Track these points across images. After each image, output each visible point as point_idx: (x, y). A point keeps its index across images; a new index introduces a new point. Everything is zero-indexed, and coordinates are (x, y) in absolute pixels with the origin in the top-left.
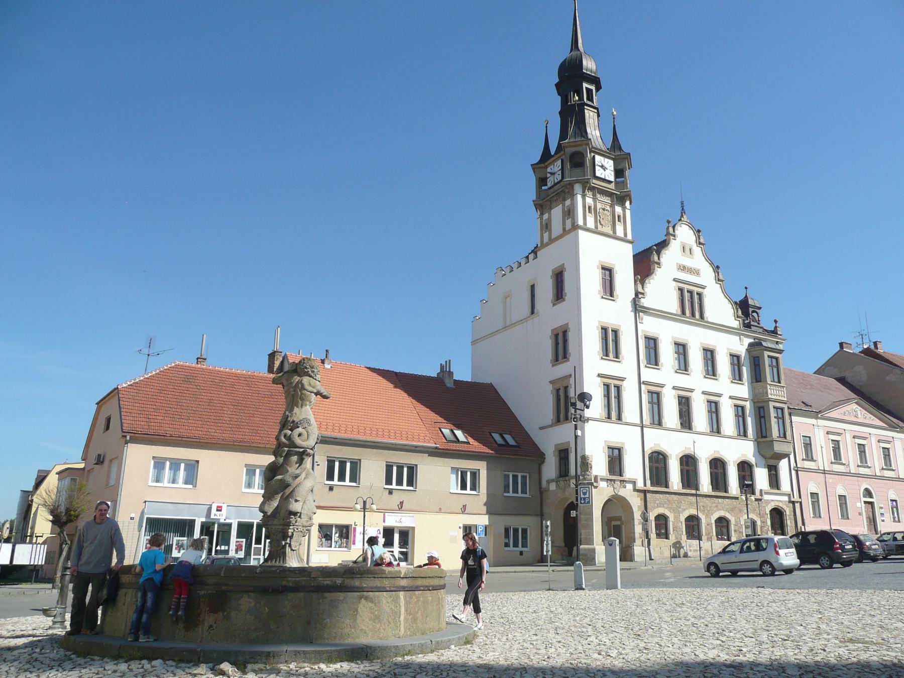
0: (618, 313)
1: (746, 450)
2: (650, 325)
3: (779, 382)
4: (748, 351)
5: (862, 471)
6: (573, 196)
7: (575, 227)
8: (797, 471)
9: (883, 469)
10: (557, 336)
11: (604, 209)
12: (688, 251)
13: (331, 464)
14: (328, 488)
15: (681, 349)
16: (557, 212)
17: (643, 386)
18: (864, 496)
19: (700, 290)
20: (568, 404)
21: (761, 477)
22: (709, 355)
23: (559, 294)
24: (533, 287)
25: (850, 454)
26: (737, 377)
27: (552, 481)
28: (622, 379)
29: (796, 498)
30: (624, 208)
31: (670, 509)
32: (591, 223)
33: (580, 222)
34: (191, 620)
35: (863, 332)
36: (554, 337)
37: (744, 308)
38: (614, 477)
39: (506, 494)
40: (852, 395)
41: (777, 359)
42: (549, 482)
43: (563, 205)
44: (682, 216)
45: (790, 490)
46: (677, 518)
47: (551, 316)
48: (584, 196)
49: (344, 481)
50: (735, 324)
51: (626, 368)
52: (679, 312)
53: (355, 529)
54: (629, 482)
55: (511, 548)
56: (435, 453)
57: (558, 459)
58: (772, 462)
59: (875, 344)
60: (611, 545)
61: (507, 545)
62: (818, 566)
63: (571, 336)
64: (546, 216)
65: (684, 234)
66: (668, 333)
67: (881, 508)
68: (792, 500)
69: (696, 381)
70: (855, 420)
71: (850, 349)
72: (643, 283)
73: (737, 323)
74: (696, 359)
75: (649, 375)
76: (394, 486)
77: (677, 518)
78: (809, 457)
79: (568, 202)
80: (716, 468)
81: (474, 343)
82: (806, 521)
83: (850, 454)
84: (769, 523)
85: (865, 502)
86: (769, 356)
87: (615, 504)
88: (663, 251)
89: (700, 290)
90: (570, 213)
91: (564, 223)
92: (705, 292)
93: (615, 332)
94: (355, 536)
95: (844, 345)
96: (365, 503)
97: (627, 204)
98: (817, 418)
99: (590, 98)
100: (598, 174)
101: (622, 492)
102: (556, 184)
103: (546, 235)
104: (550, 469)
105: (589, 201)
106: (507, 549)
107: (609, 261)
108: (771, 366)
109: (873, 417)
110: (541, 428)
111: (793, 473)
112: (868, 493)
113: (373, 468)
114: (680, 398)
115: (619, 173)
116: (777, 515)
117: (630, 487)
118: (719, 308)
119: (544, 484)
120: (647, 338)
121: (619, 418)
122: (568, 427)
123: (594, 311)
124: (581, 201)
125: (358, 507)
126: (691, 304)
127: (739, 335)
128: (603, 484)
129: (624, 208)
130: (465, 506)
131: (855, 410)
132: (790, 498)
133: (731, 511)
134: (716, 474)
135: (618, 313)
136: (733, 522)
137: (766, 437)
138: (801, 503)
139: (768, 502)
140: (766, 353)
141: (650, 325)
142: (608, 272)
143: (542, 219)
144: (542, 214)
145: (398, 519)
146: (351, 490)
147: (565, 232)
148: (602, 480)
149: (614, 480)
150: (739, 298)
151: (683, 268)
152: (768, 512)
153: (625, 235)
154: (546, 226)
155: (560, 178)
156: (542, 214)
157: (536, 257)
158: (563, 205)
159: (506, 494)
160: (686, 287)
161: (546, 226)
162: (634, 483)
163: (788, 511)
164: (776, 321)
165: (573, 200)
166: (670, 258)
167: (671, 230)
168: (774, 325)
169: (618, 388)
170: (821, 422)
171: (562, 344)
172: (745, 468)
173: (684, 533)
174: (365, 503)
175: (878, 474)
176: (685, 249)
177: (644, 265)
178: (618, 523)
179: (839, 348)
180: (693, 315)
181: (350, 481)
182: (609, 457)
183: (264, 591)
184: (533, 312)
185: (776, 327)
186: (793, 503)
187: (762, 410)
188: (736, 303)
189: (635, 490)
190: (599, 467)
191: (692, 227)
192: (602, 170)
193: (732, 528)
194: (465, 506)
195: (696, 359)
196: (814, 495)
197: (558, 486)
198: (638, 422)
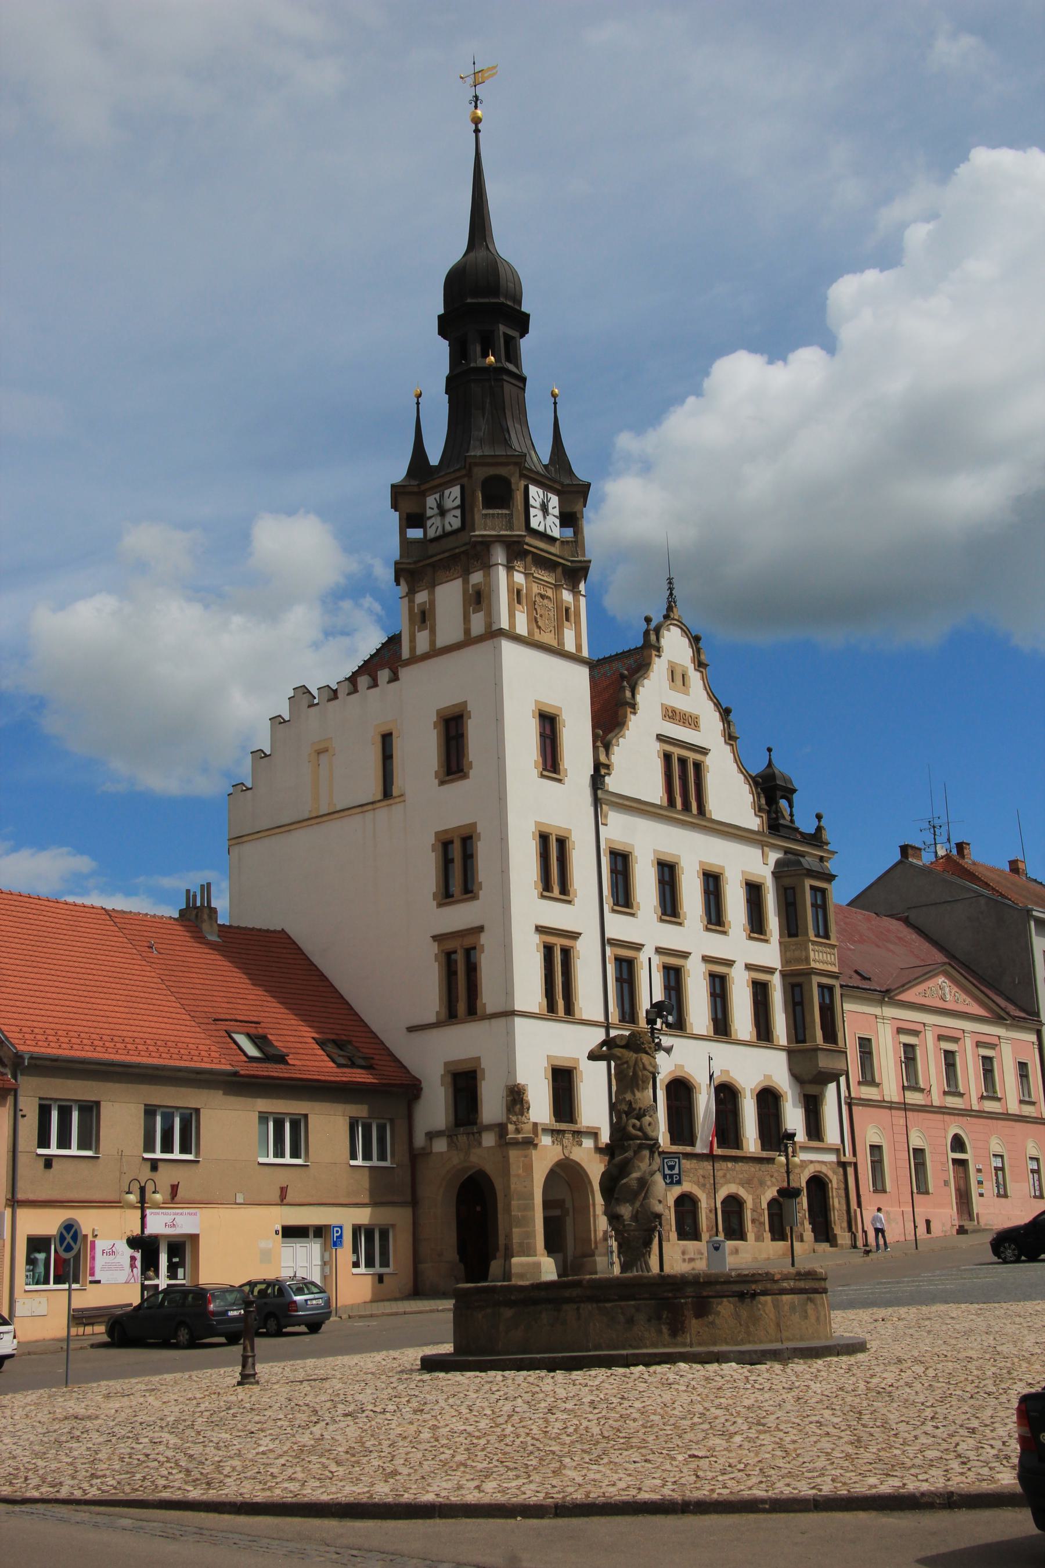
0: (566, 806)
2: (620, 829)
3: (827, 936)
4: (776, 875)
5: (952, 1102)
6: (487, 567)
8: (850, 1105)
9: (982, 1097)
11: (543, 597)
13: (44, 1112)
14: (148, 1164)
15: (668, 874)
16: (449, 596)
17: (608, 949)
18: (953, 1150)
19: (698, 757)
20: (463, 981)
21: (794, 1118)
22: (713, 883)
23: (454, 762)
24: (387, 739)
25: (931, 1069)
26: (757, 926)
27: (439, 1134)
28: (575, 936)
29: (848, 1157)
34: (677, 1329)
35: (937, 822)
37: (770, 789)
38: (563, 1126)
39: (262, 1160)
40: (940, 957)
41: (823, 891)
42: (431, 1136)
43: (466, 582)
45: (838, 1141)
46: (757, 1200)
47: (432, 805)
48: (510, 569)
49: (283, 1156)
50: (753, 822)
51: (580, 913)
52: (665, 803)
53: (93, 1244)
55: (362, 1269)
56: (238, 1084)
57: (450, 1090)
58: (812, 1090)
59: (960, 847)
60: (717, 1249)
61: (356, 1265)
63: (483, 851)
64: (421, 597)
66: (647, 841)
67: (979, 1171)
68: (843, 1159)
69: (691, 936)
70: (940, 1004)
72: (607, 747)
73: (758, 820)
75: (619, 927)
76: (53, 1150)
77: (757, 1200)
78: (869, 1079)
79: (476, 578)
83: (931, 1069)
85: (955, 1161)
86: (812, 887)
87: (566, 1174)
89: (698, 757)
90: (479, 599)
91: (466, 619)
92: (709, 761)
93: (562, 842)
94: (93, 1258)
95: (910, 851)
96: (142, 1190)
97: (582, 587)
98: (881, 1003)
100: (534, 524)
102: (446, 535)
104: (435, 1109)
105: (519, 578)
106: (356, 1271)
107: (552, 701)
108: (814, 905)
109: (968, 1000)
110: (411, 1029)
111: (844, 1108)
112: (958, 1144)
113: (122, 1117)
114: (667, 969)
115: (569, 519)
117: (588, 1143)
118: (730, 796)
119: (420, 1140)
121: (569, 1010)
123: (533, 804)
124: (504, 580)
125: (133, 1198)
126: (684, 786)
127: (762, 845)
128: (546, 1140)
129: (576, 592)
130: (283, 1191)
131: (942, 988)
132: (838, 1156)
133: (747, 1183)
135: (566, 806)
136: (749, 1204)
137: (804, 1041)
138: (855, 1164)
139: (804, 1164)
140: (809, 882)
141: (620, 829)
142: (549, 724)
143: (411, 601)
144: (411, 593)
145: (168, 1219)
146: (83, 1165)
147: (469, 641)
148: (545, 1130)
149: (563, 1132)
150: (758, 767)
151: (672, 715)
153: (579, 647)
155: (456, 523)
156: (411, 593)
158: (466, 582)
159: (353, 1163)
160: (677, 751)
161: (424, 617)
162: (595, 1135)
164: (819, 817)
165: (487, 575)
166: (653, 692)
167: (653, 637)
168: (816, 823)
169: (566, 952)
170: (890, 1012)
171: (459, 863)
173: (674, 1228)
174: (142, 1190)
175: (975, 1107)
176: (677, 678)
179: (898, 857)
180: (687, 807)
181: (80, 1148)
183: (741, 1296)
184: (387, 793)
185: (819, 829)
186: (843, 1165)
187: (797, 989)
188: (753, 779)
189: (598, 1150)
190: (540, 1107)
191: (686, 631)
193: (748, 1215)
194: (283, 1191)
196: (876, 1149)
197: (452, 1144)
198: (602, 1019)
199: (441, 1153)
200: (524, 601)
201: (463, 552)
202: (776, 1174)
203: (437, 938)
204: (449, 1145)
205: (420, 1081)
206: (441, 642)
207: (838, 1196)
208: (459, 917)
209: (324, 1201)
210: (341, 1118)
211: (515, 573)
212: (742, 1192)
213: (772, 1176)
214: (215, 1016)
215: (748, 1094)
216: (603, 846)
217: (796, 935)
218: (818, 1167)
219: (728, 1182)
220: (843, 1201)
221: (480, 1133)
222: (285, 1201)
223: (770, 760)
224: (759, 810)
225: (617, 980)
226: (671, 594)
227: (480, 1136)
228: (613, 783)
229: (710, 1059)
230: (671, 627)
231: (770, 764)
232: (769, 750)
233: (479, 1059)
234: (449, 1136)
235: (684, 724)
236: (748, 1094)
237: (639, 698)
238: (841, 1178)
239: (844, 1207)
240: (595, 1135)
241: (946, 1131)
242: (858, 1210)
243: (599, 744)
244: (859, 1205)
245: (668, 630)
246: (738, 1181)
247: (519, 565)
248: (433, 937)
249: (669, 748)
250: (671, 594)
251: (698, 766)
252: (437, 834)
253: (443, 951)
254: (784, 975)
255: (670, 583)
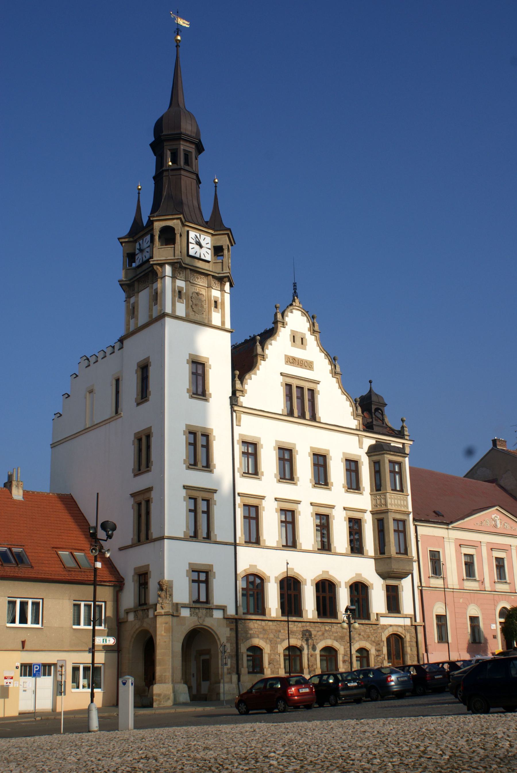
1: (365, 568)
2: (250, 427)
7: (163, 315)
10: (140, 440)
12: (298, 341)
15: (286, 456)
16: (143, 297)
17: (238, 499)
22: (320, 462)
23: (144, 394)
24: (117, 381)
26: (353, 484)
27: (184, 606)
30: (222, 290)
31: (265, 639)
32: (181, 309)
33: (168, 309)
36: (136, 442)
42: (127, 612)
44: (294, 300)
50: (354, 423)
54: (219, 608)
57: (137, 585)
62: (369, 699)
64: (132, 300)
65: (296, 321)
68: (414, 623)
69: (304, 492)
71: (505, 446)
72: (242, 378)
74: (304, 467)
77: (274, 648)
80: (324, 591)
81: (53, 446)
82: (429, 648)
84: (385, 650)
88: (268, 341)
90: (156, 298)
95: (498, 443)
99: (187, 162)
101: (208, 622)
103: (132, 322)
108: (393, 472)
111: (452, 590)
116: (396, 641)
118: (335, 404)
120: (245, 443)
122: (146, 549)
126: (301, 403)
129: (222, 290)
130: (23, 643)
134: (324, 598)
139: (385, 627)
149: (199, 608)
151: (292, 361)
152: (384, 639)
153: (223, 323)
154: (132, 312)
156: (129, 297)
157: (121, 348)
159: (75, 627)
161: (132, 312)
163: (408, 638)
164: (403, 421)
166: (277, 349)
168: (401, 424)
171: (145, 450)
172: (359, 590)
176: (298, 340)
177: (245, 359)
178: (207, 657)
181: (20, 622)
182: (147, 588)
184: (117, 412)
185: (403, 427)
192: (197, 247)
193: (340, 658)
194: (23, 643)
195: (304, 467)
197: (136, 616)
198: (233, 541)
199: (132, 621)
200: (183, 297)
201: (150, 271)
202: (362, 633)
203: (133, 495)
204: (135, 617)
205: (123, 579)
206: (141, 323)
207: (411, 646)
208: (143, 482)
209: (34, 649)
210: (67, 601)
211: (213, 290)
212: (336, 645)
213: (360, 634)
214: (52, 546)
215: (343, 585)
216: (236, 438)
217: (380, 490)
218: (395, 629)
219: (361, 639)
220: (415, 649)
221: (148, 609)
222: (24, 649)
223: (371, 387)
224: (355, 415)
225: (245, 517)
226: (295, 292)
227: (148, 611)
228: (243, 400)
229: (288, 564)
230: (294, 311)
231: (371, 391)
232: (370, 382)
233: (148, 565)
234: (135, 611)
235: (301, 366)
236: (343, 585)
237: (267, 352)
238: (414, 635)
239: (416, 653)
240: (223, 609)
241: (495, 606)
242: (425, 655)
243: (237, 379)
244: (426, 651)
245: (292, 312)
246: (333, 637)
247: (182, 275)
248: (131, 495)
249: (289, 381)
250: (295, 292)
251: (312, 392)
252: (135, 434)
253: (135, 502)
254: (373, 513)
255: (295, 286)
